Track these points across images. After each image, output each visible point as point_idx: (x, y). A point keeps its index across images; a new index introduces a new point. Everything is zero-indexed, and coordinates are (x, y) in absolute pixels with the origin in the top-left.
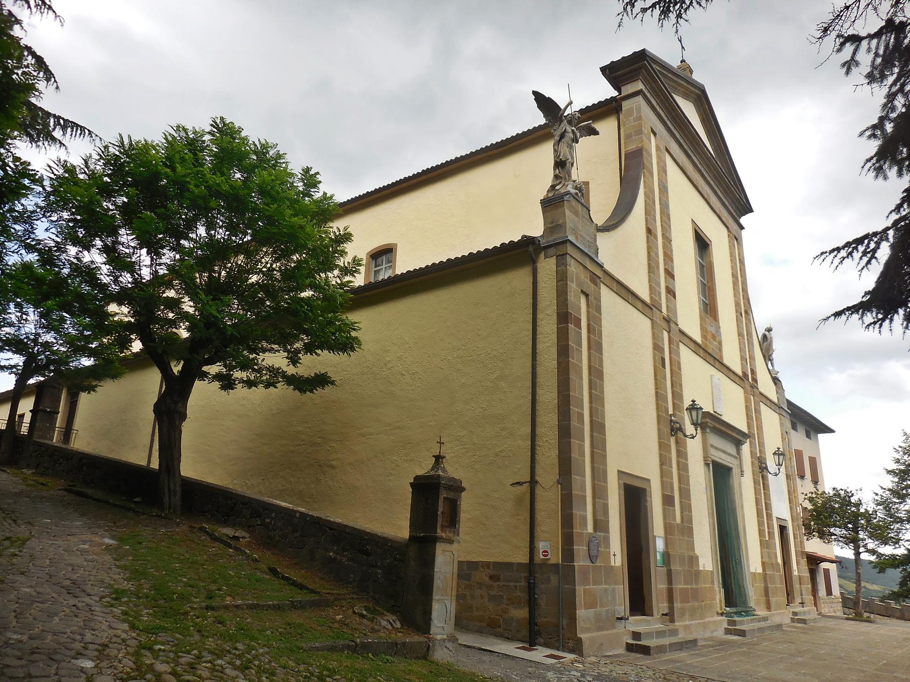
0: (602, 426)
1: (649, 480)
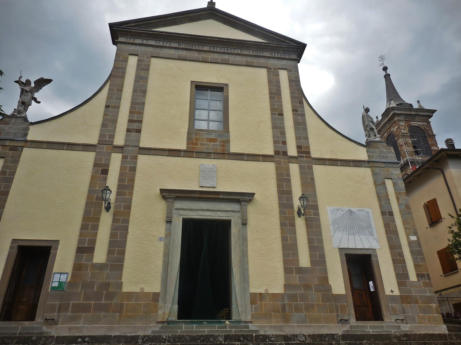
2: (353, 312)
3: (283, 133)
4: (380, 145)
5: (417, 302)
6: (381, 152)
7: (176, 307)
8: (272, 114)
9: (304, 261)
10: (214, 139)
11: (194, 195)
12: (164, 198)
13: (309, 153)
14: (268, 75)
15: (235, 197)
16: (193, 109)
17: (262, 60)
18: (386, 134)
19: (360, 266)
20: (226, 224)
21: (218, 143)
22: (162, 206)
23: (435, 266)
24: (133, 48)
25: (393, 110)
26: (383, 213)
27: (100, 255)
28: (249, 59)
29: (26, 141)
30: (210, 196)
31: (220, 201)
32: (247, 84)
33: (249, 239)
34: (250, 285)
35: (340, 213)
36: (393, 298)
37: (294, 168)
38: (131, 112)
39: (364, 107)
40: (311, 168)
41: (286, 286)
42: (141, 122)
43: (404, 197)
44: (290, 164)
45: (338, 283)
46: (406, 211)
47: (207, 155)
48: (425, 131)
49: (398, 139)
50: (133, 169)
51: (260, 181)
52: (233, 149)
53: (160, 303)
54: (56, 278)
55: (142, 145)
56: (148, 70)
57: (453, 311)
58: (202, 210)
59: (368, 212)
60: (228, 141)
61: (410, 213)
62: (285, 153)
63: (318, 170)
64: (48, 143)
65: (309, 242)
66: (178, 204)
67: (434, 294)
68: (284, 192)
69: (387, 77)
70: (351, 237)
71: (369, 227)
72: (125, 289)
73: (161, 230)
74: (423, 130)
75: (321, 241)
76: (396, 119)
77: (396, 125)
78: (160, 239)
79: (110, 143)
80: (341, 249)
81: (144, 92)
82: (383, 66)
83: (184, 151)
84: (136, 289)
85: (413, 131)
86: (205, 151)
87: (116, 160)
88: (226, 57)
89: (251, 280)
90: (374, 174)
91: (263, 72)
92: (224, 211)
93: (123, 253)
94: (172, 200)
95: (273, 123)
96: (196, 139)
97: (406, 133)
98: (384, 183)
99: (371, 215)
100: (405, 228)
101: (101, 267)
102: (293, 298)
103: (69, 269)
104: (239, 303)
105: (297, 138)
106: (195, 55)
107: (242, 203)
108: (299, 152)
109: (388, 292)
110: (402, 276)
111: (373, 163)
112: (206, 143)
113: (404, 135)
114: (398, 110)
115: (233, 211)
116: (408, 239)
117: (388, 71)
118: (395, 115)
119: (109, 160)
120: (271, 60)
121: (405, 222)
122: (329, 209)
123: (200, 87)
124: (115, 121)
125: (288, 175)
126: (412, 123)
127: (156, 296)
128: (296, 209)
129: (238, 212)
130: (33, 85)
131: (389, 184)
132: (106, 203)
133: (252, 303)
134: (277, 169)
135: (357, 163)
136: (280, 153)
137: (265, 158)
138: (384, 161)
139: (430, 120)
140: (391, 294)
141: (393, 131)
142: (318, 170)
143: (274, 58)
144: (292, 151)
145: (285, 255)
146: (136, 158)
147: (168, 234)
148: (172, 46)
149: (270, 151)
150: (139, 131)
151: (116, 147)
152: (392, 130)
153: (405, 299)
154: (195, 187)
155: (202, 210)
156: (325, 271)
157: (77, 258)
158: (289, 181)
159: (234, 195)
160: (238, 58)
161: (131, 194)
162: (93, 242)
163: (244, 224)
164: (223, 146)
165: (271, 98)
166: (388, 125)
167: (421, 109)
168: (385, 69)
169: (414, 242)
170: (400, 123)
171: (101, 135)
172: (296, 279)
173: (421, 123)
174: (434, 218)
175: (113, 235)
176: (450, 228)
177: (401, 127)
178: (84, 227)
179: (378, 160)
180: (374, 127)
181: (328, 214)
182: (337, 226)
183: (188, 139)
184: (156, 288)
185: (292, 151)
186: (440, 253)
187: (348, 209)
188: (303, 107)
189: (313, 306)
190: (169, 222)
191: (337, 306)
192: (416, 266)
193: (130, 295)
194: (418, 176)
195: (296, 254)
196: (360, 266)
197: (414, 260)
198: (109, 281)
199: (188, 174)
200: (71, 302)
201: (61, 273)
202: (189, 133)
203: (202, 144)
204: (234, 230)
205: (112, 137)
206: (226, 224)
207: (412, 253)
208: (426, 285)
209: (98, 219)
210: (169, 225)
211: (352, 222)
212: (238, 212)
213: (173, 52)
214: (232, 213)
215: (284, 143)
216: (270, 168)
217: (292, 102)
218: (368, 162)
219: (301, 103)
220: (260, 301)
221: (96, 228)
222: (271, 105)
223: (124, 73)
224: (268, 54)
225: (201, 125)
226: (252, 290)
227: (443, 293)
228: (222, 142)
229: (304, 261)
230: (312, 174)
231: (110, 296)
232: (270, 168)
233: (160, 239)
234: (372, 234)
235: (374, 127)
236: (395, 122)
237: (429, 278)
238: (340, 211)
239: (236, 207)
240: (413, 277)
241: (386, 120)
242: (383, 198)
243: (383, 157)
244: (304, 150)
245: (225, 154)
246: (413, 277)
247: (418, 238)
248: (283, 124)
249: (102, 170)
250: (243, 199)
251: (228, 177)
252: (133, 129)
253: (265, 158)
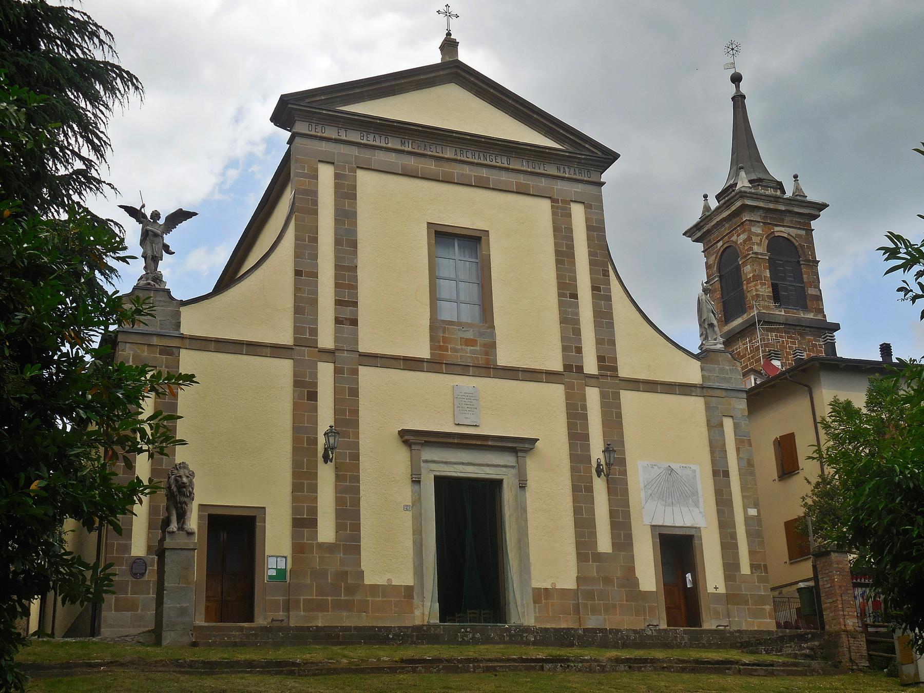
2: (664, 615)
3: (577, 332)
4: (721, 357)
5: (746, 603)
6: (722, 370)
7: (437, 606)
8: (560, 295)
9: (604, 544)
10: (473, 340)
11: (451, 441)
12: (407, 443)
13: (615, 369)
14: (554, 214)
15: (510, 445)
16: (434, 278)
17: (543, 182)
18: (720, 244)
19: (677, 549)
20: (495, 485)
21: (478, 348)
22: (401, 457)
23: (779, 543)
24: (324, 146)
25: (742, 197)
26: (715, 473)
27: (326, 531)
28: (522, 179)
29: (183, 337)
30: (474, 442)
31: (485, 450)
32: (516, 225)
33: (529, 510)
34: (533, 576)
35: (656, 471)
36: (716, 597)
37: (593, 395)
38: (337, 285)
40: (617, 396)
41: (578, 579)
42: (355, 304)
43: (744, 423)
44: (587, 388)
45: (648, 577)
46: (743, 442)
47: (462, 369)
48: (799, 249)
49: (745, 264)
50: (354, 392)
51: (536, 415)
52: (503, 359)
53: (416, 601)
54: (272, 563)
55: (362, 349)
56: (354, 197)
57: (795, 617)
58: (463, 464)
59: (694, 471)
60: (493, 345)
61: (752, 474)
62: (580, 369)
63: (627, 398)
64: (218, 341)
65: (611, 516)
66: (428, 454)
67: (769, 593)
68: (578, 437)
69: (739, 100)
70: (669, 509)
71: (695, 493)
72: (367, 581)
73: (405, 493)
74: (796, 247)
75: (627, 514)
76: (746, 217)
77: (744, 231)
78: (406, 508)
79: (313, 344)
80: (653, 527)
81: (354, 244)
82: (732, 71)
83: (428, 361)
84: (381, 580)
85: (777, 245)
86: (459, 361)
87: (325, 372)
88: (484, 172)
89: (533, 570)
90: (708, 408)
91: (546, 204)
92: (494, 466)
93: (357, 527)
94: (419, 447)
95: (561, 312)
96: (445, 340)
97: (762, 254)
98: (721, 425)
99: (698, 476)
100: (743, 497)
101: (330, 548)
102: (590, 595)
103: (287, 550)
104: (519, 602)
105: (599, 342)
106: (431, 166)
107: (520, 454)
108: (600, 368)
109: (710, 589)
110: (730, 567)
111: (709, 390)
112: (460, 347)
113: (756, 258)
114: (752, 198)
115: (506, 466)
116: (745, 512)
117: (744, 87)
118: (744, 208)
119: (315, 375)
120: (559, 182)
121: (744, 488)
122: (641, 464)
123: (442, 236)
124: (314, 302)
125: (584, 407)
126: (777, 229)
127: (409, 590)
128: (594, 465)
129: (513, 467)
130: (161, 221)
131: (728, 424)
132: (326, 449)
133: (535, 602)
134: (568, 396)
135: (684, 389)
136: (573, 368)
137: (550, 376)
138: (724, 386)
139: (813, 224)
140: (714, 591)
141: (736, 243)
142: (627, 398)
143: (563, 178)
144: (591, 366)
145: (578, 535)
146: (355, 372)
147: (417, 500)
148: (390, 145)
149: (557, 365)
150: (354, 322)
151: (325, 354)
152: (734, 238)
153: (732, 598)
154: (448, 427)
155: (463, 464)
156: (632, 559)
157: (295, 535)
158: (585, 417)
159: (509, 442)
160: (504, 177)
161: (357, 435)
162: (314, 511)
163: (523, 487)
164: (487, 354)
165: (558, 262)
166: (727, 225)
167: (799, 200)
168: (736, 79)
169: (753, 517)
170: (753, 229)
171: (297, 330)
172: (592, 569)
173: (793, 232)
174: (787, 465)
175: (339, 501)
176: (803, 499)
177: (754, 240)
178: (296, 488)
179: (716, 385)
180: (715, 322)
181: (639, 473)
182: (650, 492)
183: (433, 339)
184: (406, 578)
185: (591, 366)
186: (789, 525)
187: (665, 464)
188: (608, 283)
189: (614, 606)
190: (416, 482)
191: (644, 607)
192: (752, 553)
193: (374, 588)
194: (773, 386)
195: (593, 534)
196: (677, 549)
197: (750, 544)
198: (346, 569)
199: (434, 402)
200: (302, 598)
201: (277, 557)
202: (433, 328)
203: (454, 350)
204: (508, 495)
205: (314, 332)
206: (495, 485)
207: (749, 534)
208: (761, 580)
209: (315, 476)
210: (417, 487)
211: (672, 488)
212: (513, 467)
213: (392, 158)
214: (504, 469)
215: (579, 350)
216: (556, 393)
217: (592, 272)
218: (702, 387)
219: (606, 274)
220: (546, 599)
221: (314, 489)
222: (559, 277)
223: (315, 203)
224: (552, 170)
225: (448, 312)
226: (535, 584)
227: (785, 590)
228: (485, 345)
229: (604, 544)
230: (619, 406)
231: (351, 590)
232: (556, 393)
233: (406, 508)
234: (696, 505)
235: (715, 322)
236: (742, 223)
237: (766, 571)
238: (656, 468)
239: (509, 459)
240: (745, 569)
241: (725, 214)
242: (717, 449)
243: (724, 378)
244: (607, 363)
245: (489, 368)
246: (745, 569)
247: (758, 512)
248: (577, 314)
249: (306, 392)
250: (519, 447)
251: (501, 408)
252: (346, 319)
253: (550, 376)
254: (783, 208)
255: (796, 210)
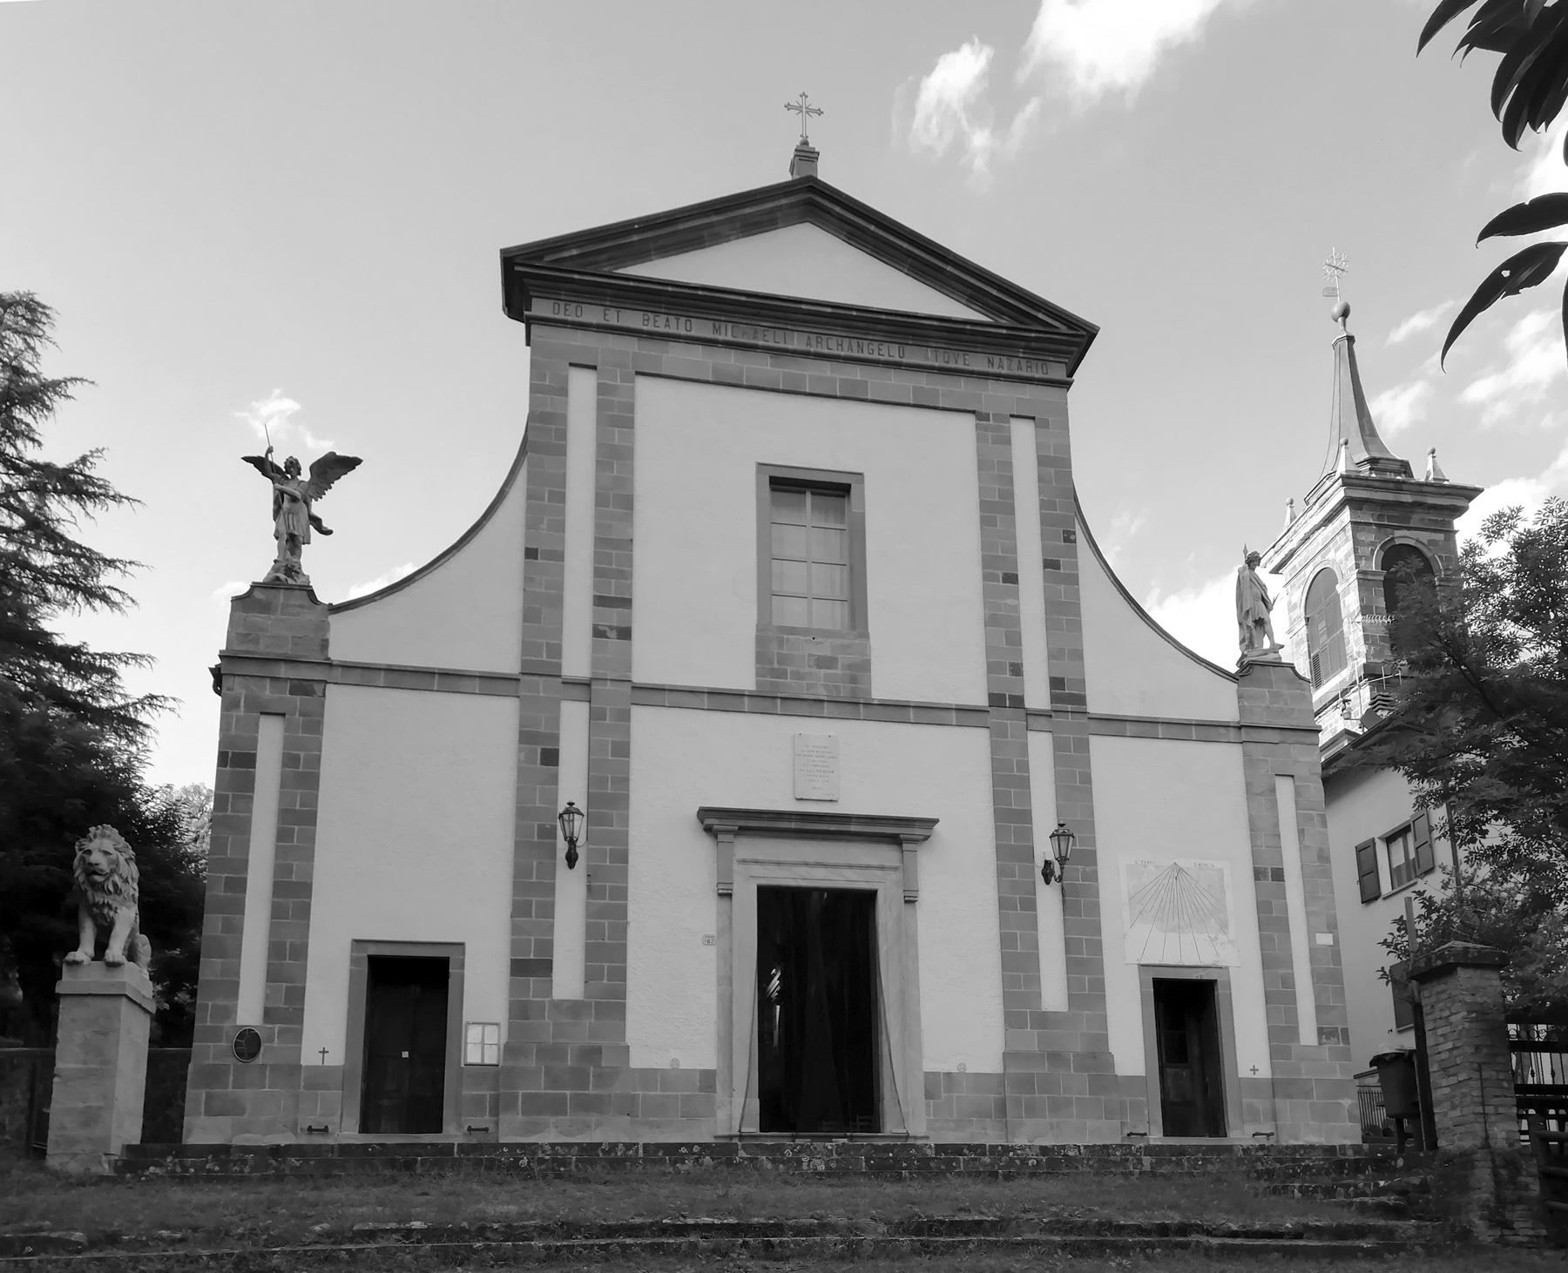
0: (305, 889)
1: (462, 944)
18: (1310, 567)
39: (1245, 551)
97: (1373, 573)
126: (1398, 533)
152: (1331, 556)
254: (1407, 498)
255: (1431, 500)
